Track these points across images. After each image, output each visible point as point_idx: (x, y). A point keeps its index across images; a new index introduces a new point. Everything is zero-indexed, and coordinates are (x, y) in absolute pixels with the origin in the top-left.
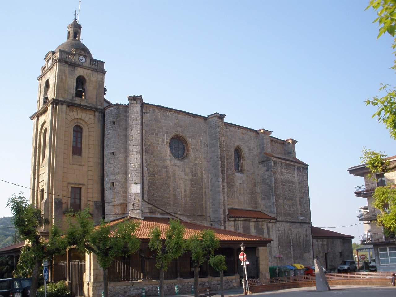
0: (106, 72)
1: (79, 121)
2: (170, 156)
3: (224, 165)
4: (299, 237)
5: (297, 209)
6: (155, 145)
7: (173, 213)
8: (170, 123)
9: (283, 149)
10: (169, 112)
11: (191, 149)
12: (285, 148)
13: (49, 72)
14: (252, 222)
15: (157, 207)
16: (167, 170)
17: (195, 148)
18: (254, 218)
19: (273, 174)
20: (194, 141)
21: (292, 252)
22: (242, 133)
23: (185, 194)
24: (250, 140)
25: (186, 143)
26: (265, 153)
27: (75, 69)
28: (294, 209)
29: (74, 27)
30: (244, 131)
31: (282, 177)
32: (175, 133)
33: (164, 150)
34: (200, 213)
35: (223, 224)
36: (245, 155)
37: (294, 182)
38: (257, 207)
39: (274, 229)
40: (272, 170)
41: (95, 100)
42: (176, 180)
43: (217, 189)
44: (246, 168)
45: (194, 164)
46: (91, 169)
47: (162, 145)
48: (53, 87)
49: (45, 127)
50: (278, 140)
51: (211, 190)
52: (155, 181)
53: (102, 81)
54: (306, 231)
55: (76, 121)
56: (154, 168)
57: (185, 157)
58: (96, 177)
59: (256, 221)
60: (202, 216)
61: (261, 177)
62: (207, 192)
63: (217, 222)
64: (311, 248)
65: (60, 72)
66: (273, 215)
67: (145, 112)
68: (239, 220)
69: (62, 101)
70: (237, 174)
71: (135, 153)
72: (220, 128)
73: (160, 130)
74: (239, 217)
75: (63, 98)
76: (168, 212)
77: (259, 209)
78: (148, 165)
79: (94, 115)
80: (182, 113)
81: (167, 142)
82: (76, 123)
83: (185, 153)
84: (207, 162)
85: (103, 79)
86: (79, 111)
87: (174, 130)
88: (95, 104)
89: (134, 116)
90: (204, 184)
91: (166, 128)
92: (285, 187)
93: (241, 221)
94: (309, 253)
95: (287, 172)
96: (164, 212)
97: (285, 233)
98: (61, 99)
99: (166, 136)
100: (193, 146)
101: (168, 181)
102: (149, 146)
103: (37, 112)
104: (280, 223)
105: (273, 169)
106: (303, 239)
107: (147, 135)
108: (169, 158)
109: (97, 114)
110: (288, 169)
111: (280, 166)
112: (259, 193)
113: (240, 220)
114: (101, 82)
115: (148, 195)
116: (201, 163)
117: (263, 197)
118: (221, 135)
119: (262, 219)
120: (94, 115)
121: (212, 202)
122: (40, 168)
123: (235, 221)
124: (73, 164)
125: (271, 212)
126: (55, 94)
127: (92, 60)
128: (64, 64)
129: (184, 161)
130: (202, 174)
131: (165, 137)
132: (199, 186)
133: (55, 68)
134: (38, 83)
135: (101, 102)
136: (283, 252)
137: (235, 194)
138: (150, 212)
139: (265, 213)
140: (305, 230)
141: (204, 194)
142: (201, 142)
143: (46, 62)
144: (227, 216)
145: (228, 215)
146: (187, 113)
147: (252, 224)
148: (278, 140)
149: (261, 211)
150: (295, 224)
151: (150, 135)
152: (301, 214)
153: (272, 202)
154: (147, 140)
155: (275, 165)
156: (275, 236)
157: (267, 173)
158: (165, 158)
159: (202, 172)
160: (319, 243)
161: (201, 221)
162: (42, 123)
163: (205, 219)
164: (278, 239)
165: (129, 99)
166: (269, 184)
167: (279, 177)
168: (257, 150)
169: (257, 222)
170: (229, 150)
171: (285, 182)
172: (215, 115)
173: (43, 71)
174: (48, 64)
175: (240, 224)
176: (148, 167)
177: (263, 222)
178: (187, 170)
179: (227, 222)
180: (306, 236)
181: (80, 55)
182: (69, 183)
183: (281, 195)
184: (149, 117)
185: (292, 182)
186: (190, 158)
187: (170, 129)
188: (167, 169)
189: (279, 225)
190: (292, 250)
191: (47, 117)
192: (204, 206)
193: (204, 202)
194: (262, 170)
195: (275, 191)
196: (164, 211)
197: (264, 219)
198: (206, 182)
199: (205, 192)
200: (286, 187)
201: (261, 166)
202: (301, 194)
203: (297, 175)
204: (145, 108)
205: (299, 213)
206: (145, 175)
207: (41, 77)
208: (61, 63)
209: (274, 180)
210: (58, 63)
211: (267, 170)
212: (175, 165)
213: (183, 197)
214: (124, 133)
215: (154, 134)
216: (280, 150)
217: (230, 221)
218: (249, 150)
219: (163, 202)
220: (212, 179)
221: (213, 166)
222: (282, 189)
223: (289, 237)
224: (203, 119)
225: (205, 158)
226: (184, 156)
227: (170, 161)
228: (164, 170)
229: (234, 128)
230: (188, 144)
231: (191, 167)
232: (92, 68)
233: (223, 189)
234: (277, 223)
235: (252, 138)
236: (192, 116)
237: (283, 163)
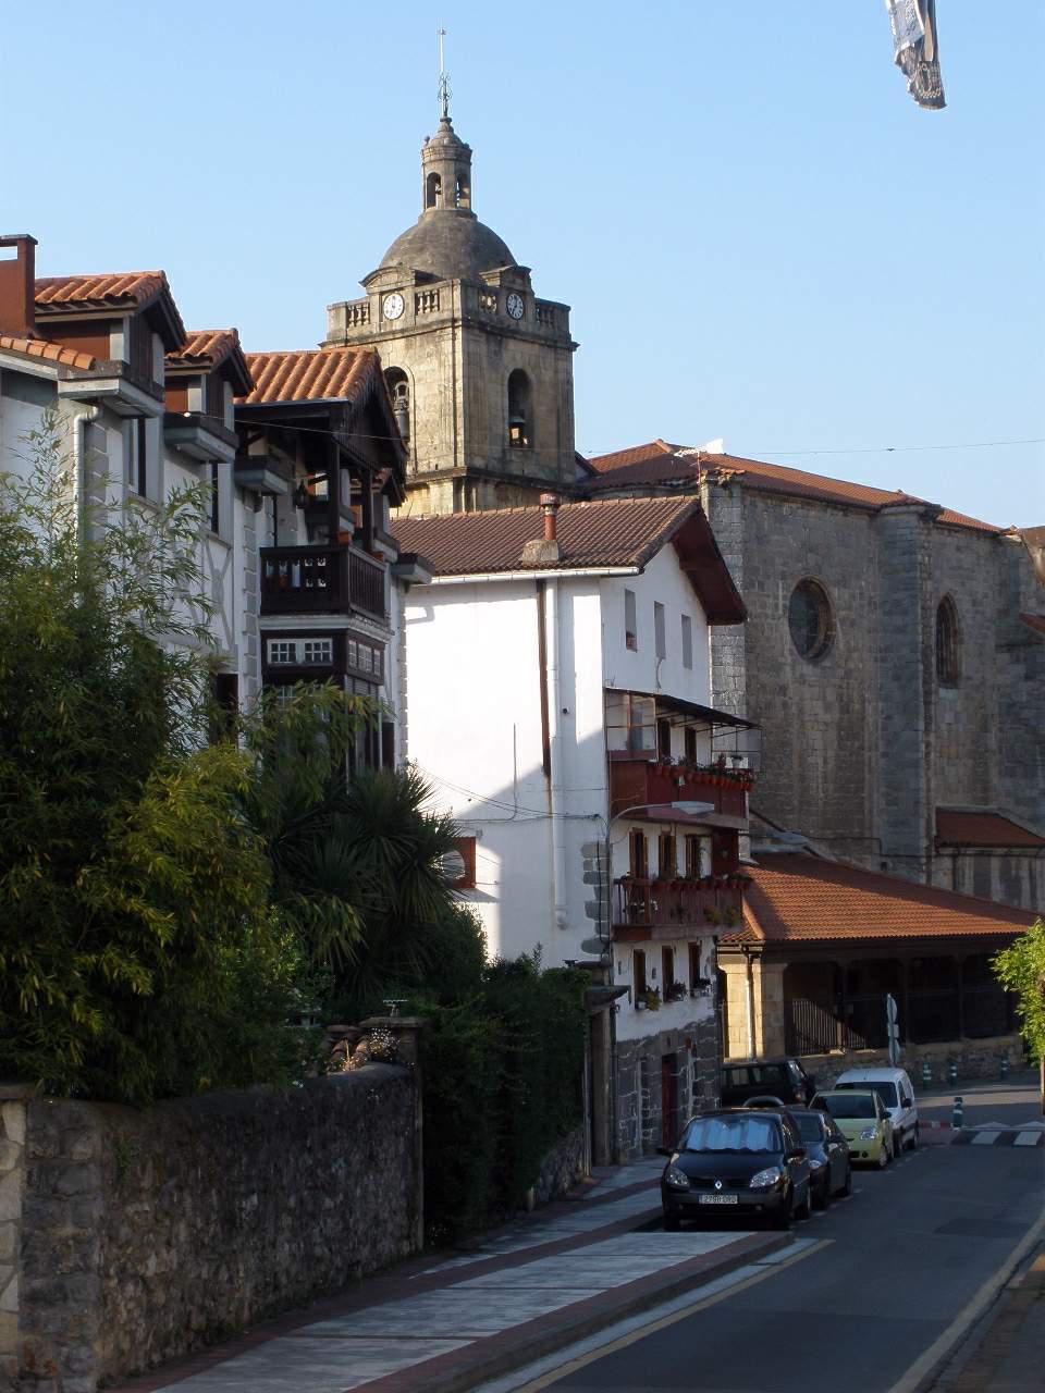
0: (576, 345)
15: (765, 820)
26: (1023, 617)
27: (504, 345)
29: (456, 160)
38: (986, 801)
51: (885, 755)
65: (469, 364)
68: (965, 855)
70: (943, 692)
74: (969, 845)
77: (992, 807)
83: (821, 637)
100: (843, 613)
116: (861, 666)
117: (1007, 764)
123: (954, 857)
128: (476, 332)
131: (780, 590)
132: (857, 744)
139: (1013, 819)
141: (866, 769)
142: (861, 594)
147: (995, 864)
149: (997, 814)
157: (1025, 686)
159: (863, 696)
175: (968, 865)
179: (933, 860)
188: (785, 695)
192: (867, 804)
201: (1006, 657)
211: (1028, 677)
212: (802, 680)
217: (943, 855)
218: (974, 603)
221: (897, 678)
227: (793, 668)
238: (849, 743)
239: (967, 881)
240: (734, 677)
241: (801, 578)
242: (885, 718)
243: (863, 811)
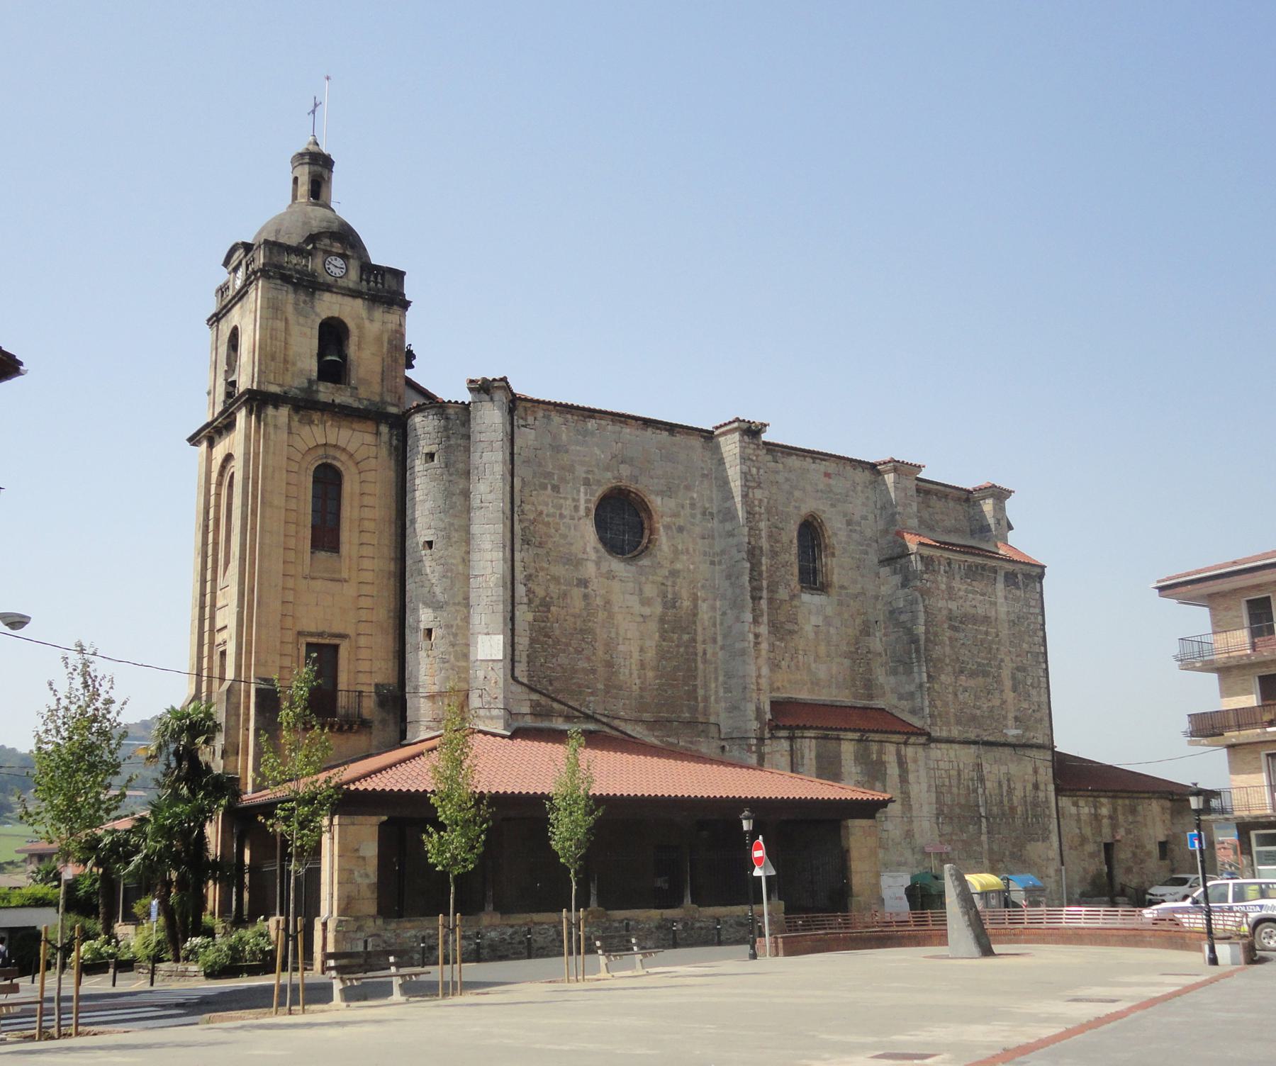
1: (331, 452)
3: (760, 574)
4: (1010, 791)
5: (1004, 702)
6: (550, 519)
7: (605, 715)
8: (598, 452)
9: (965, 516)
10: (594, 421)
11: (661, 528)
12: (972, 512)
13: (238, 306)
14: (847, 743)
15: (554, 700)
16: (587, 591)
17: (675, 525)
18: (854, 730)
19: (922, 596)
20: (672, 503)
21: (984, 838)
22: (827, 475)
23: (641, 660)
24: (851, 493)
25: (647, 510)
27: (317, 296)
28: (990, 704)
30: (831, 467)
31: (953, 605)
32: (614, 483)
34: (687, 715)
35: (754, 748)
36: (834, 541)
37: (993, 619)
38: (871, 697)
39: (921, 763)
40: (918, 583)
41: (376, 388)
42: (613, 619)
43: (738, 646)
44: (835, 579)
46: (366, 589)
47: (572, 518)
48: (249, 353)
49: (232, 471)
50: (948, 490)
51: (722, 648)
52: (548, 624)
53: (397, 331)
54: (1036, 771)
55: (321, 451)
56: (548, 587)
57: (643, 551)
58: (383, 613)
59: (859, 741)
60: (691, 723)
61: (885, 604)
62: (709, 652)
63: (737, 741)
64: (1053, 826)
66: (916, 722)
70: (806, 597)
71: (488, 546)
73: (567, 474)
74: (805, 728)
75: (280, 385)
76: (588, 712)
77: (879, 703)
78: (529, 577)
79: (377, 434)
80: (634, 421)
82: (321, 459)
83: (645, 541)
84: (712, 563)
85: (401, 325)
86: (329, 423)
87: (609, 475)
88: (377, 399)
89: (483, 437)
90: (700, 630)
91: (584, 469)
92: (962, 635)
93: (810, 738)
94: (1043, 841)
95: (970, 588)
96: (577, 714)
97: (959, 775)
98: (274, 389)
99: (586, 494)
100: (593, 498)
101: (590, 624)
102: (533, 522)
103: (208, 425)
104: (943, 746)
105: (921, 580)
106: (1025, 796)
107: (527, 491)
108: (593, 556)
109: (384, 429)
110: (972, 580)
111: (945, 572)
112: (880, 654)
113: (806, 738)
115: (528, 663)
116: (692, 567)
118: (752, 484)
119: (882, 732)
120: (378, 433)
121: (725, 683)
122: (218, 589)
123: (791, 739)
124: (313, 578)
125: (913, 712)
126: (256, 375)
127: (369, 270)
128: (279, 282)
129: (641, 563)
130: (695, 599)
131: (582, 495)
132: (686, 637)
133: (254, 294)
134: (208, 334)
135: (396, 393)
136: (954, 837)
137: (800, 657)
138: (534, 714)
140: (1030, 770)
141: (699, 659)
143: (230, 273)
144: (769, 724)
145: (769, 720)
146: (647, 423)
148: (948, 490)
150: (995, 749)
151: (535, 490)
152: (1016, 719)
153: (917, 681)
154: (527, 507)
155: (927, 569)
156: (924, 786)
157: (901, 593)
158: (580, 556)
159: (695, 594)
160: (1082, 812)
161: (689, 739)
162: (224, 456)
163: (703, 731)
164: (934, 795)
165: (471, 390)
166: (909, 626)
167: (941, 604)
168: (876, 522)
169: (863, 744)
170: (780, 526)
171: (957, 622)
172: (736, 425)
173: (222, 301)
174: (234, 280)
176: (529, 585)
177: (886, 742)
178: (650, 591)
179: (767, 742)
180: (1036, 787)
181: (329, 253)
182: (300, 633)
183: (947, 661)
185: (986, 619)
186: (658, 553)
187: (596, 470)
188: (586, 587)
189: (937, 752)
190: (984, 829)
191: (236, 443)
192: (701, 692)
193: (699, 682)
194: (889, 582)
195: (925, 650)
196: (577, 710)
197: (886, 732)
198: (707, 623)
199: (705, 653)
200: (966, 636)
201: (885, 571)
202: (1017, 656)
203: (1006, 598)
204: (520, 411)
205: (1011, 715)
206: (520, 606)
207: (216, 319)
208: (271, 280)
209: (923, 614)
210: (260, 282)
211: (904, 586)
212: (610, 576)
213: (634, 667)
214: (461, 487)
215: (549, 487)
216: (956, 520)
218: (849, 523)
219: (575, 684)
220: (724, 614)
222: (950, 643)
223: (975, 791)
224: (702, 436)
225: (705, 554)
226: (639, 548)
227: (598, 564)
228: (577, 593)
229: (802, 458)
230: (653, 513)
231: (661, 579)
233: (757, 644)
234: (933, 745)
235: (859, 488)
236: (666, 430)
237: (956, 560)
238: (676, 636)
239: (806, 761)
240: (492, 561)
241: (610, 485)
242: (722, 615)
243: (697, 698)
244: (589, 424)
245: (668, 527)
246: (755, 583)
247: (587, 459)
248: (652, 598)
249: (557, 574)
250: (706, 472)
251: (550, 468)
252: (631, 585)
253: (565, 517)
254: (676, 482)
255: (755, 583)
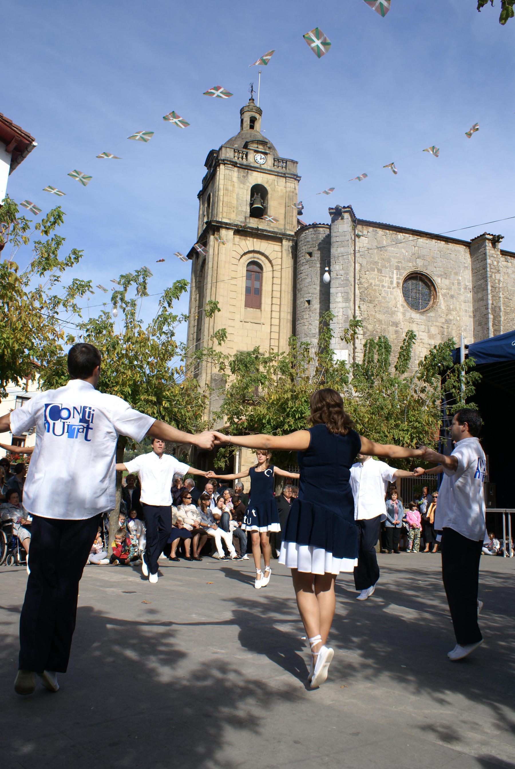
2: (403, 307)
6: (377, 288)
10: (402, 234)
11: (441, 295)
16: (397, 329)
20: (447, 282)
32: (413, 269)
33: (393, 297)
45: (446, 320)
47: (389, 288)
55: (251, 255)
67: (360, 234)
69: (226, 224)
72: (492, 259)
73: (386, 263)
75: (229, 219)
81: (398, 283)
87: (410, 264)
91: (397, 260)
99: (397, 274)
108: (401, 309)
114: (291, 194)
116: (458, 318)
129: (429, 315)
151: (368, 271)
154: (363, 281)
158: (394, 309)
165: (331, 213)
178: (434, 330)
184: (367, 242)
187: (403, 261)
188: (397, 327)
215: (376, 270)
227: (404, 314)
232: (278, 172)
236: (444, 241)
244: (399, 236)
245: (444, 295)
246: (496, 327)
247: (398, 255)
248: (435, 335)
249: (381, 318)
250: (466, 265)
251: (376, 259)
252: (423, 327)
253: (385, 287)
254: (449, 270)
255: (496, 327)
